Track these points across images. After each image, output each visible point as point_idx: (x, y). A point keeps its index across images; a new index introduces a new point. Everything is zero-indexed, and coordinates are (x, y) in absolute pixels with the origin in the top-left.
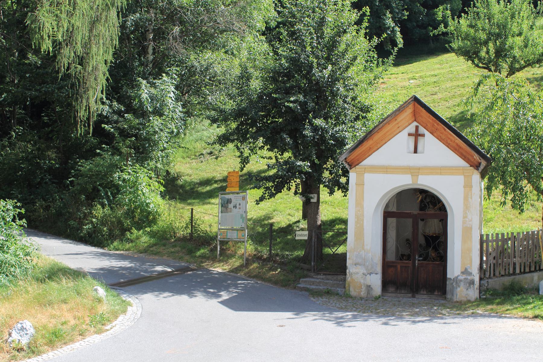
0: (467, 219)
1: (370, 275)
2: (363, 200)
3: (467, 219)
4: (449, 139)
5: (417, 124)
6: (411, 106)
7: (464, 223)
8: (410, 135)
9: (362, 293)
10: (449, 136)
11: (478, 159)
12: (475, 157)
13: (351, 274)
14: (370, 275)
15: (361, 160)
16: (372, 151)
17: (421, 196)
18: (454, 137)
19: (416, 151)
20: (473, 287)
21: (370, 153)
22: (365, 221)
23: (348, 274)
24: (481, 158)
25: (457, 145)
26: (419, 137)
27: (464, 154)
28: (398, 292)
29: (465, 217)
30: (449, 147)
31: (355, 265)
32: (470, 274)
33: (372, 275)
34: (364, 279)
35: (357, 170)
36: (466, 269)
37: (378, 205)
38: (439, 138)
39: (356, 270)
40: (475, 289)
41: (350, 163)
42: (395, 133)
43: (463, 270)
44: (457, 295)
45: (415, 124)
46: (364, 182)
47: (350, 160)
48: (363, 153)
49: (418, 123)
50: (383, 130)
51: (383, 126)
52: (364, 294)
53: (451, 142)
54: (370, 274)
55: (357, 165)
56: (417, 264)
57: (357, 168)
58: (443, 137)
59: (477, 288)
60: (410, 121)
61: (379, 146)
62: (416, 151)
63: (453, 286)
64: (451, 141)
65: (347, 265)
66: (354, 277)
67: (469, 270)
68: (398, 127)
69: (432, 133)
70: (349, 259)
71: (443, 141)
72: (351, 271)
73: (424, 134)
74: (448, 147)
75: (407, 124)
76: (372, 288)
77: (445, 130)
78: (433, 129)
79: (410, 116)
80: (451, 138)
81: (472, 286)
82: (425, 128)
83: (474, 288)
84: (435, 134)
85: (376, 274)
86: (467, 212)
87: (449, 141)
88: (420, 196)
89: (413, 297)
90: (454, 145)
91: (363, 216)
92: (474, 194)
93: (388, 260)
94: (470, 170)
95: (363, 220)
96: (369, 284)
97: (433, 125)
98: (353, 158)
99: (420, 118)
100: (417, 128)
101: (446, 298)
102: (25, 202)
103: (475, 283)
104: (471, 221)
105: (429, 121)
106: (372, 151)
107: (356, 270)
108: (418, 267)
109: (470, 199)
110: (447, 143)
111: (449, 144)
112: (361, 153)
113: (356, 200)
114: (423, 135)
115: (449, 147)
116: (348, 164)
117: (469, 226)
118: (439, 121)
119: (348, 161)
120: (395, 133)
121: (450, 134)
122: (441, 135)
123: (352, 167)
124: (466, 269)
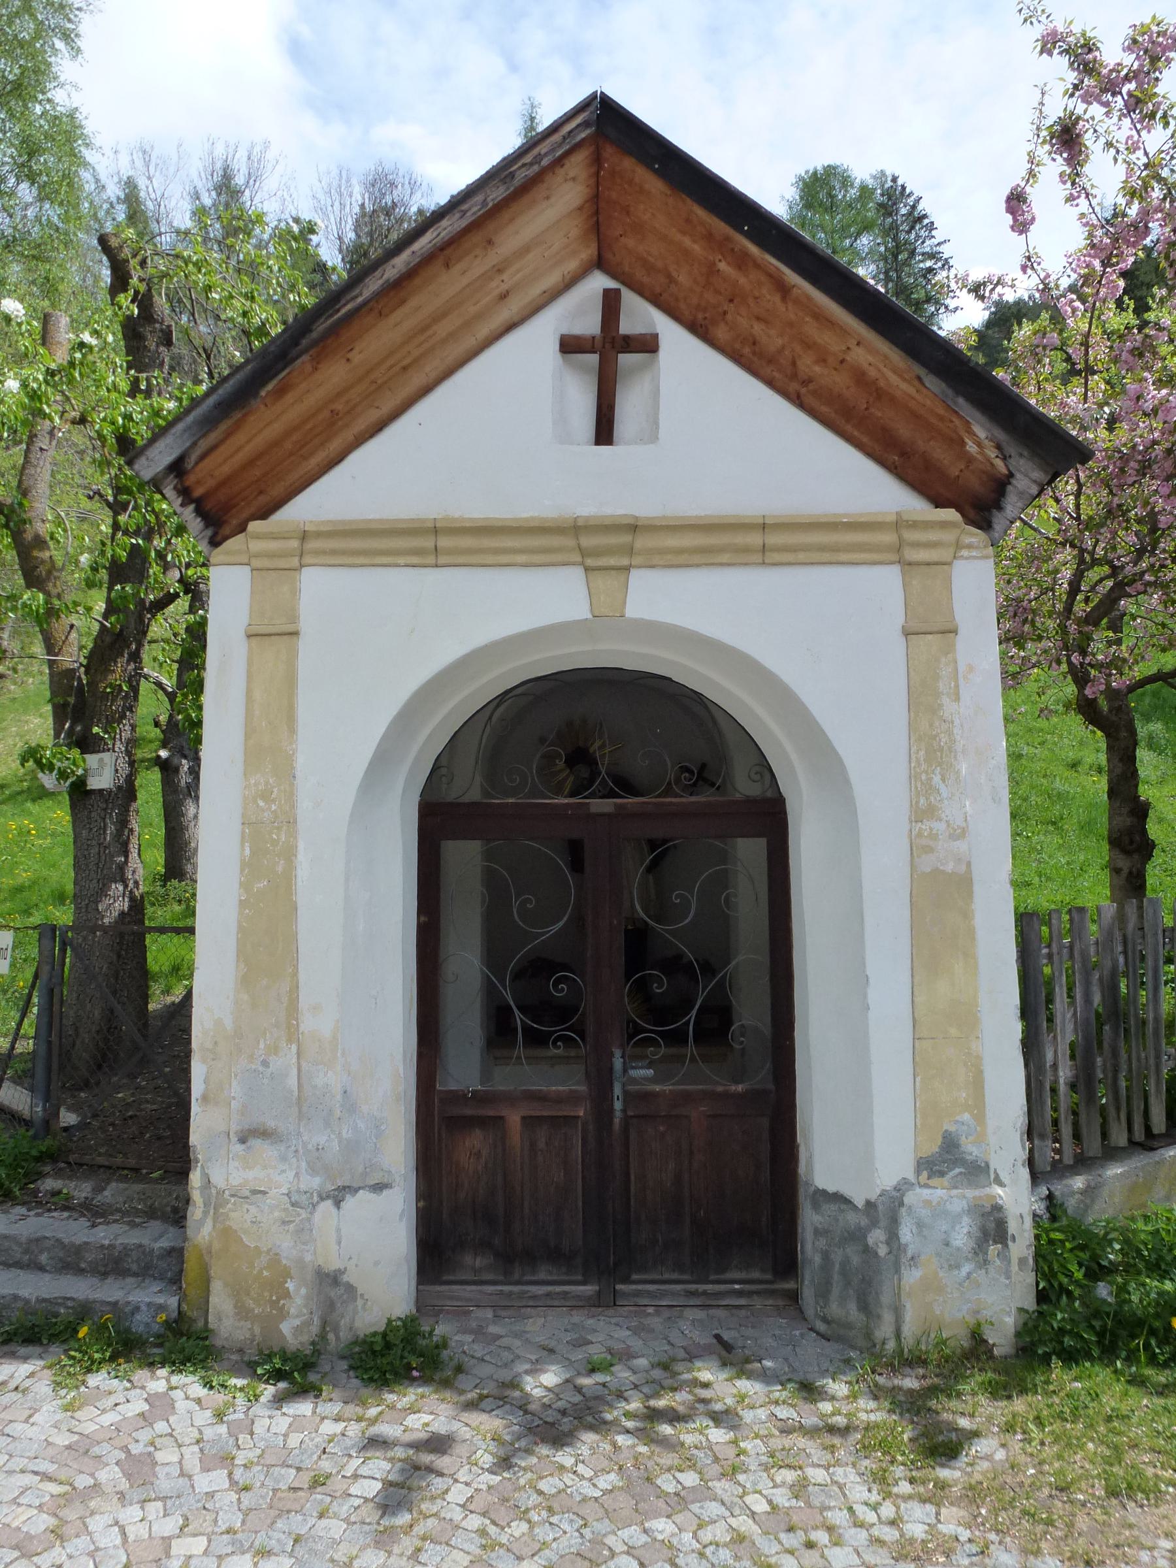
0: (939, 827)
1: (338, 1203)
2: (292, 731)
3: (939, 827)
4: (809, 345)
5: (611, 284)
6: (578, 165)
7: (918, 848)
8: (570, 346)
9: (286, 1328)
10: (811, 329)
11: (992, 453)
12: (971, 447)
13: (216, 1202)
14: (338, 1203)
15: (277, 491)
16: (349, 435)
17: (571, 779)
18: (843, 332)
19: (604, 433)
20: (1004, 1256)
21: (335, 445)
22: (303, 858)
23: (196, 1196)
24: (1011, 450)
25: (860, 378)
26: (625, 359)
27: (904, 431)
28: (516, 1276)
29: (922, 812)
30: (809, 400)
31: (243, 1141)
32: (978, 1172)
33: (350, 1202)
34: (299, 1231)
35: (256, 546)
36: (950, 1145)
37: (382, 760)
38: (747, 350)
39: (250, 1175)
40: (1015, 1268)
41: (208, 506)
42: (484, 330)
43: (932, 1147)
44: (898, 1312)
45: (599, 282)
46: (294, 618)
47: (211, 483)
48: (288, 445)
49: (614, 276)
50: (413, 303)
51: (410, 274)
52: (297, 1330)
53: (817, 369)
54: (338, 1196)
55: (264, 514)
56: (618, 1105)
57: (258, 537)
58: (772, 340)
59: (1022, 1261)
60: (572, 265)
61: (388, 405)
62: (604, 433)
63: (868, 1252)
64: (822, 360)
65: (194, 1139)
66: (239, 1217)
67: (970, 1149)
68: (504, 296)
69: (699, 329)
70: (205, 1098)
71: (768, 371)
72: (218, 1179)
73: (655, 337)
74: (798, 402)
75: (552, 279)
76: (350, 1289)
77: (784, 290)
78: (710, 297)
79: (575, 232)
80: (826, 338)
81: (993, 1249)
82: (656, 301)
83: (1007, 1260)
84: (721, 333)
85: (379, 1188)
86: (937, 779)
87: (807, 364)
88: (565, 779)
89: (605, 1301)
90: (839, 381)
91: (292, 822)
92: (971, 669)
93: (453, 1086)
94: (944, 525)
95: (290, 854)
96: (334, 1264)
97: (712, 271)
98: (226, 469)
99: (630, 242)
100: (611, 304)
101: (794, 1297)
102: (128, 914)
103: (1012, 1227)
104: (960, 834)
105: (686, 253)
106: (349, 435)
107: (250, 1175)
108: (626, 1120)
109: (945, 700)
110: (794, 376)
111: (806, 382)
112: (276, 443)
113: (250, 731)
114: (648, 345)
115: (809, 400)
116: (199, 512)
117: (950, 867)
118: (748, 235)
119: (198, 492)
120: (484, 330)
121: (820, 317)
122: (758, 329)
123: (226, 530)
124: (950, 1145)
